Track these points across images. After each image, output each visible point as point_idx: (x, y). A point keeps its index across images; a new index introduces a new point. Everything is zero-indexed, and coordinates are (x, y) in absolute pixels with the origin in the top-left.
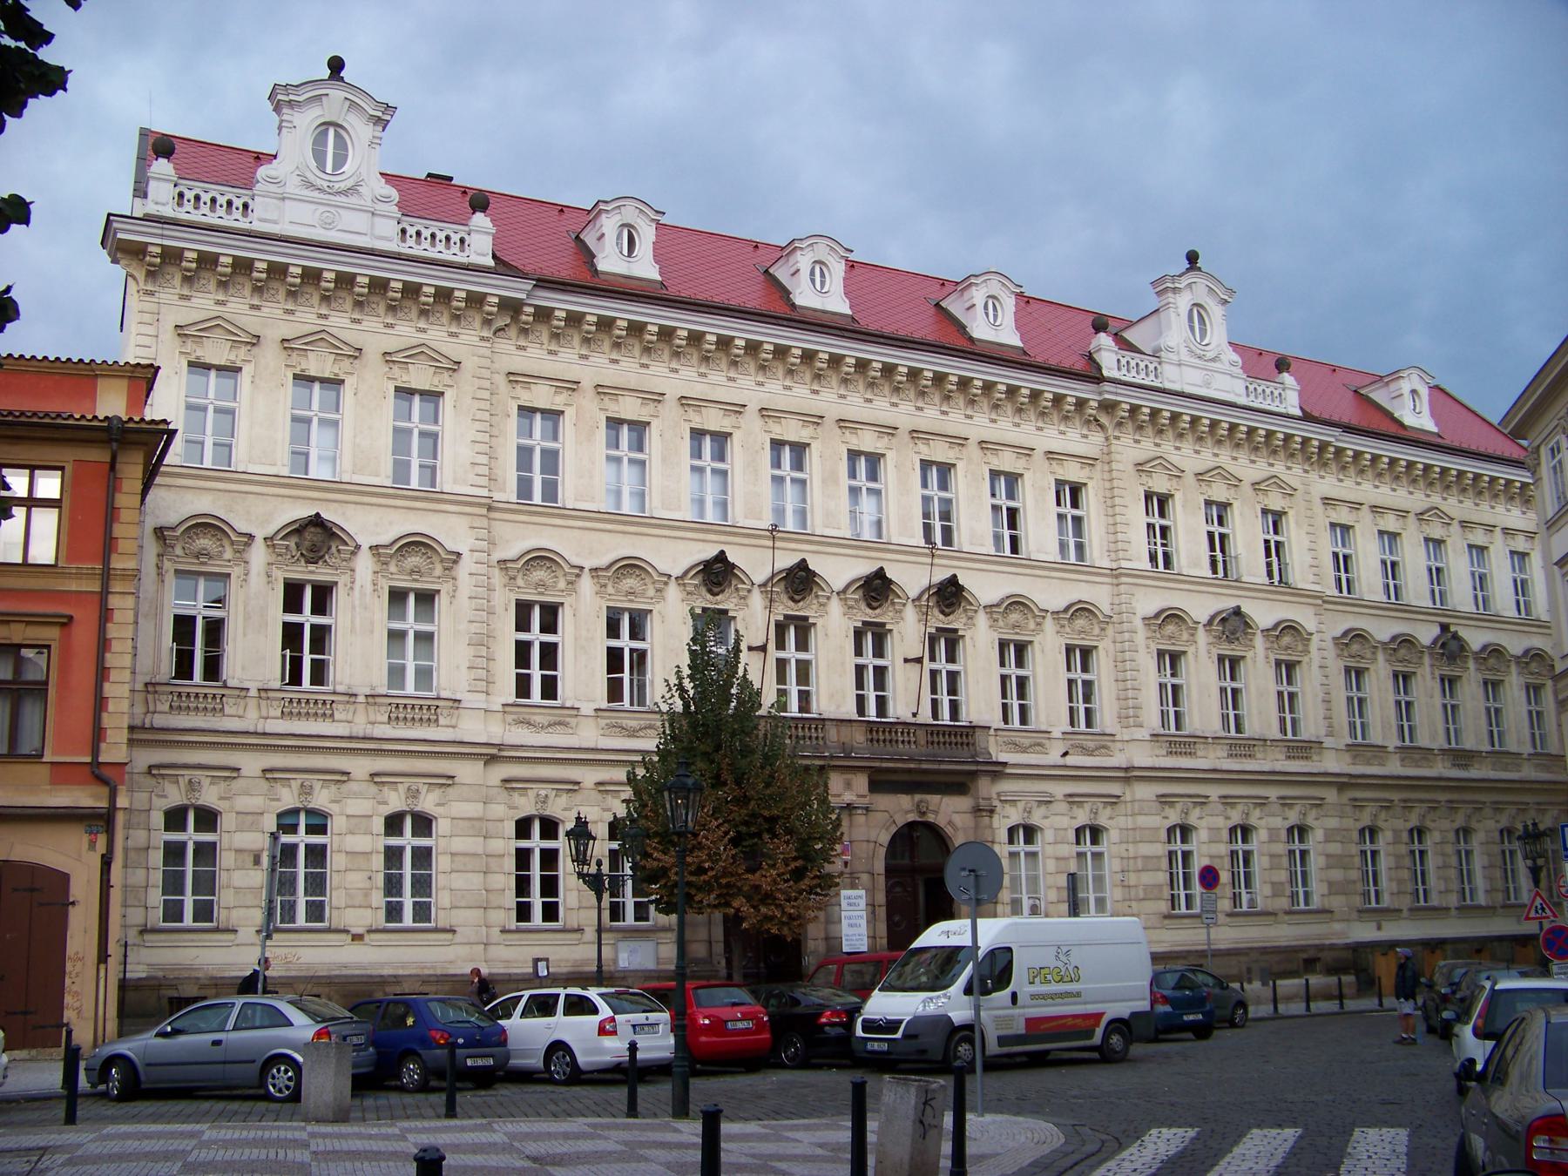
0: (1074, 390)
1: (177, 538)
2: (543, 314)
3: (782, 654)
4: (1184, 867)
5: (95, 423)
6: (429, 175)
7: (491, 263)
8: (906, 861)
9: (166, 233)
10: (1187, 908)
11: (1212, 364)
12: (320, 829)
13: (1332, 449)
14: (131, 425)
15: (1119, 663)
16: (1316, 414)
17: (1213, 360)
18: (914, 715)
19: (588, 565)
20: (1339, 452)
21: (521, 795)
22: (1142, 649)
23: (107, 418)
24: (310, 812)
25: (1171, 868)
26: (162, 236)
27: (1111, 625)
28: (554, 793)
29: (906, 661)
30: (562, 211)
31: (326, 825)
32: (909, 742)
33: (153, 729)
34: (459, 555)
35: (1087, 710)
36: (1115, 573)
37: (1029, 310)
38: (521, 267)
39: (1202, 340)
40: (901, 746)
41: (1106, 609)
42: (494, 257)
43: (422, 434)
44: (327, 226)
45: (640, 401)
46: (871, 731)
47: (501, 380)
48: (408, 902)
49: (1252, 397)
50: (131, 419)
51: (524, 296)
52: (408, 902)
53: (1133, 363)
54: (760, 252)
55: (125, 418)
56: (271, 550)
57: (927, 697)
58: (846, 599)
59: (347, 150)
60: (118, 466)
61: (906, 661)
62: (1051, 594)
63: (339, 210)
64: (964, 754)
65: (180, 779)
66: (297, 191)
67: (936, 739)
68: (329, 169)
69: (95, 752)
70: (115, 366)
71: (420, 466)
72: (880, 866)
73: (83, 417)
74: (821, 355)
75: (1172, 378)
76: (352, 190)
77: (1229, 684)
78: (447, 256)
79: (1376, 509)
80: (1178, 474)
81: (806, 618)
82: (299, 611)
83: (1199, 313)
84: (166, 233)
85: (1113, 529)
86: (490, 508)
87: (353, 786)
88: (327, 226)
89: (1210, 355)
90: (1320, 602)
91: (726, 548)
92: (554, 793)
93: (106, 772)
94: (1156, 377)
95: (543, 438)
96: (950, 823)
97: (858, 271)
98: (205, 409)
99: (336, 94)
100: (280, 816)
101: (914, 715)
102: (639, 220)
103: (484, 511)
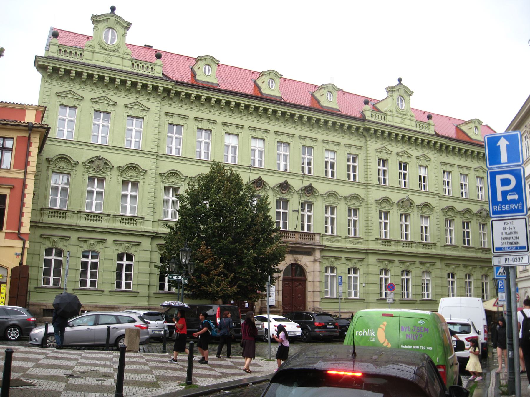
0: (355, 124)
1: (54, 161)
2: (178, 94)
3: (303, 213)
4: (406, 284)
5: (24, 124)
6: (145, 45)
7: (161, 75)
9: (54, 62)
10: (407, 297)
11: (404, 116)
12: (97, 257)
13: (445, 146)
14: (36, 125)
15: (367, 214)
16: (440, 134)
17: (405, 115)
18: (295, 229)
19: (189, 176)
20: (447, 147)
21: (85, 243)
23: (28, 123)
24: (93, 252)
25: (402, 284)
26: (53, 63)
28: (96, 243)
30: (188, 59)
31: (98, 256)
32: (293, 238)
33: (42, 223)
34: (146, 171)
35: (332, 228)
36: (367, 185)
37: (344, 96)
38: (171, 78)
39: (401, 108)
40: (290, 238)
41: (363, 197)
42: (163, 74)
43: (205, 143)
47: (163, 114)
48: (123, 282)
49: (418, 127)
50: (35, 123)
51: (171, 87)
52: (123, 282)
53: (377, 115)
54: (286, 82)
55: (34, 123)
57: (300, 223)
58: (274, 190)
59: (115, 37)
60: (31, 138)
61: (293, 211)
62: (344, 191)
64: (311, 242)
65: (51, 239)
66: (98, 50)
67: (302, 237)
68: (400, 108)
69: (19, 229)
70: (32, 106)
71: (102, 137)
73: (20, 122)
74: (313, 119)
75: (389, 120)
76: (116, 50)
77: (404, 223)
78: (147, 73)
79: (459, 166)
80: (390, 153)
81: (310, 202)
82: (280, 208)
83: (401, 99)
84: (54, 62)
85: (366, 171)
86: (157, 156)
88: (108, 62)
89: (404, 113)
90: (437, 197)
92: (96, 243)
93: (22, 237)
94: (385, 120)
95: (205, 138)
96: (305, 264)
97: (287, 82)
98: (64, 120)
99: (112, 19)
100: (83, 252)
101: (295, 229)
103: (155, 157)
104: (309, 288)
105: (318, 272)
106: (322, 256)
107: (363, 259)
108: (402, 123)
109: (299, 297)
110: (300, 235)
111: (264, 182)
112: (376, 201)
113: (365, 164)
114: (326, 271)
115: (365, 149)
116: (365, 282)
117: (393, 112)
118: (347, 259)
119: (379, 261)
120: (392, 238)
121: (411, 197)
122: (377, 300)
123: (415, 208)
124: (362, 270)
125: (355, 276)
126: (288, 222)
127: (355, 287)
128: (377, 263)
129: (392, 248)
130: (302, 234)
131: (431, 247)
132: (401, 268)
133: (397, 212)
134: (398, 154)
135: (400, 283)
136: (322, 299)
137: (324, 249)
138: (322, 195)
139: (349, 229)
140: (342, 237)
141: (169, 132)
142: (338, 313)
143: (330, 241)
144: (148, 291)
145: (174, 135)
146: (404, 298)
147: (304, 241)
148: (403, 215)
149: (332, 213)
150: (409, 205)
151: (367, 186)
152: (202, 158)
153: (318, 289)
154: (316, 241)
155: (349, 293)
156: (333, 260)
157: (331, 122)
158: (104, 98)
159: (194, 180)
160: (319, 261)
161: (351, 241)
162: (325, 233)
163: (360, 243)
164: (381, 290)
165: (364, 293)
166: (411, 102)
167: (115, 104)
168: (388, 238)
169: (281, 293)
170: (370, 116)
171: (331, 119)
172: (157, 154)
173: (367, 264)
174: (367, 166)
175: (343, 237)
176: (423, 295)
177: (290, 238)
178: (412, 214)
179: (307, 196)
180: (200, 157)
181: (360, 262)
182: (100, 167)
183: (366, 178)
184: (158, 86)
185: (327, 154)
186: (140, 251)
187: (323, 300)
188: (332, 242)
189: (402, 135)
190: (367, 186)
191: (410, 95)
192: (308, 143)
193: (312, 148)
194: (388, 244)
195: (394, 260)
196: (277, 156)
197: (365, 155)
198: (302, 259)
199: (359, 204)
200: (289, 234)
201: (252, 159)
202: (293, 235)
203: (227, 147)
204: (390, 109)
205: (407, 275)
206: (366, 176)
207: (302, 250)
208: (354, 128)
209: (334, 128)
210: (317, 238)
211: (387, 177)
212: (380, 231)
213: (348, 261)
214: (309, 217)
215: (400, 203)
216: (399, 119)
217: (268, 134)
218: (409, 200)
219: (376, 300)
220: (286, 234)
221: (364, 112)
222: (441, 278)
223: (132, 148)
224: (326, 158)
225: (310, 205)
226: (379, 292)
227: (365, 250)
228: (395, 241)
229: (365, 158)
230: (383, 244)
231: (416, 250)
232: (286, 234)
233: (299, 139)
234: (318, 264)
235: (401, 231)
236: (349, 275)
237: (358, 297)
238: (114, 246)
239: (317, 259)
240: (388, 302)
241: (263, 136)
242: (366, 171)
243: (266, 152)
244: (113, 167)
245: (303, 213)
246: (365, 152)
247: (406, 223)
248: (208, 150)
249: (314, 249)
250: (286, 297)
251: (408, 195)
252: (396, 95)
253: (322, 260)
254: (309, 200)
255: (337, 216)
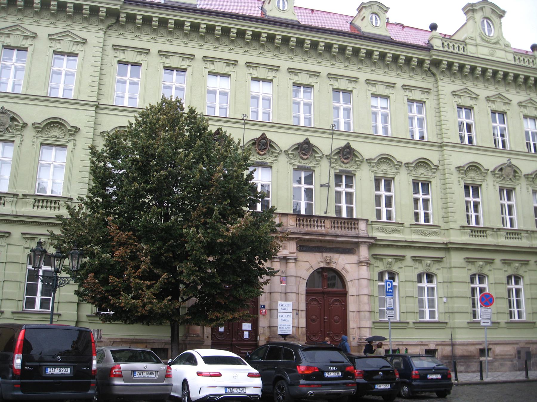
3: (338, 189)
8: (321, 289)
10: (519, 318)
11: (495, 45)
15: (444, 189)
18: (326, 213)
22: (456, 182)
25: (509, 296)
27: (438, 172)
29: (322, 186)
32: (321, 226)
36: (441, 146)
40: (316, 228)
41: (436, 163)
44: (492, 55)
45: (385, 86)
46: (299, 220)
51: (119, 8)
56: (459, 172)
58: (288, 154)
63: (496, 50)
64: (352, 232)
66: (480, 43)
67: (336, 225)
68: (487, 34)
72: (303, 289)
77: (506, 202)
80: (476, 97)
81: (349, 172)
82: (469, 196)
83: (487, 21)
85: (439, 124)
87: (405, 263)
89: (493, 41)
91: (309, 137)
96: (344, 268)
102: (379, 12)
104: (352, 306)
105: (366, 281)
106: (372, 255)
107: (442, 258)
108: (492, 55)
109: (336, 321)
110: (334, 223)
111: (271, 141)
112: (458, 168)
113: (438, 115)
114: (420, 281)
115: (436, 93)
116: (446, 296)
117: (476, 40)
118: (415, 259)
119: (469, 262)
120: (487, 225)
121: (514, 162)
122: (468, 323)
123: (523, 179)
124: (441, 276)
125: (430, 285)
126: (313, 203)
127: (431, 303)
128: (464, 264)
129: (489, 240)
130: (337, 220)
131: (519, 237)
132: (505, 271)
133: (494, 185)
134: (488, 99)
135: (506, 296)
136: (374, 323)
137: (374, 244)
138: (369, 161)
139: (468, 216)
140: (405, 225)
141: (119, 74)
142: (402, 345)
143: (384, 231)
144: (76, 313)
145: (128, 78)
146: (513, 319)
147: (339, 232)
148: (503, 190)
149: (388, 189)
150: (512, 173)
151: (441, 147)
152: (302, 123)
153: (366, 308)
154: (361, 232)
155: (421, 313)
156: (390, 260)
157: (378, 53)
158: (66, 34)
159: (39, 128)
160: (367, 263)
161: (420, 231)
162: (375, 219)
163: (435, 233)
164: (510, 307)
165: (445, 313)
166: (503, 26)
167: (34, 36)
168: (481, 225)
169: (303, 314)
170: (441, 45)
171: (377, 49)
172: (97, 103)
173: (449, 267)
174: (440, 117)
175: (407, 224)
176: (511, 314)
177: (316, 228)
178: (518, 188)
179: (343, 162)
180: (257, 118)
181: (399, 262)
182: (510, 175)
183: (440, 133)
184: (261, 33)
185: (374, 102)
186: (9, 246)
187: (376, 325)
188: (389, 232)
189: (482, 68)
190: (441, 147)
191: (501, 17)
192: (343, 84)
193: (350, 92)
194: (482, 234)
195: (493, 260)
196: (408, 121)
197: (436, 102)
198: (338, 259)
199: (430, 174)
200: (314, 221)
201: (373, 126)
202: (321, 222)
203: (336, 111)
204: (472, 36)
205: (517, 283)
206: (439, 132)
207: (338, 246)
208: (402, 59)
209: (409, 67)
210: (362, 226)
211: (473, 134)
212: (503, 218)
213: (417, 263)
214: (349, 196)
215: (497, 172)
216: (486, 49)
217: (278, 73)
218: (510, 166)
219: (466, 324)
220: (310, 221)
221: (431, 42)
222: (296, 277)
223: (259, 120)
224: (375, 107)
225: (350, 178)
226: (507, 310)
227: (443, 244)
228: (493, 229)
229: (436, 106)
230: (474, 234)
231: (529, 242)
232: (310, 221)
233: (328, 79)
234: (365, 268)
235: (502, 214)
236: (420, 285)
237: (436, 319)
238: (23, 242)
239: (362, 259)
240: (482, 324)
241: (387, 92)
242: (439, 124)
243: (428, 118)
244: (281, 151)
245: (338, 189)
246: (435, 98)
247: (510, 203)
248: (310, 113)
249: (357, 244)
250: (313, 321)
251: (263, 132)
252: (478, 16)
253: (372, 261)
254: (348, 169)
255: (395, 193)
